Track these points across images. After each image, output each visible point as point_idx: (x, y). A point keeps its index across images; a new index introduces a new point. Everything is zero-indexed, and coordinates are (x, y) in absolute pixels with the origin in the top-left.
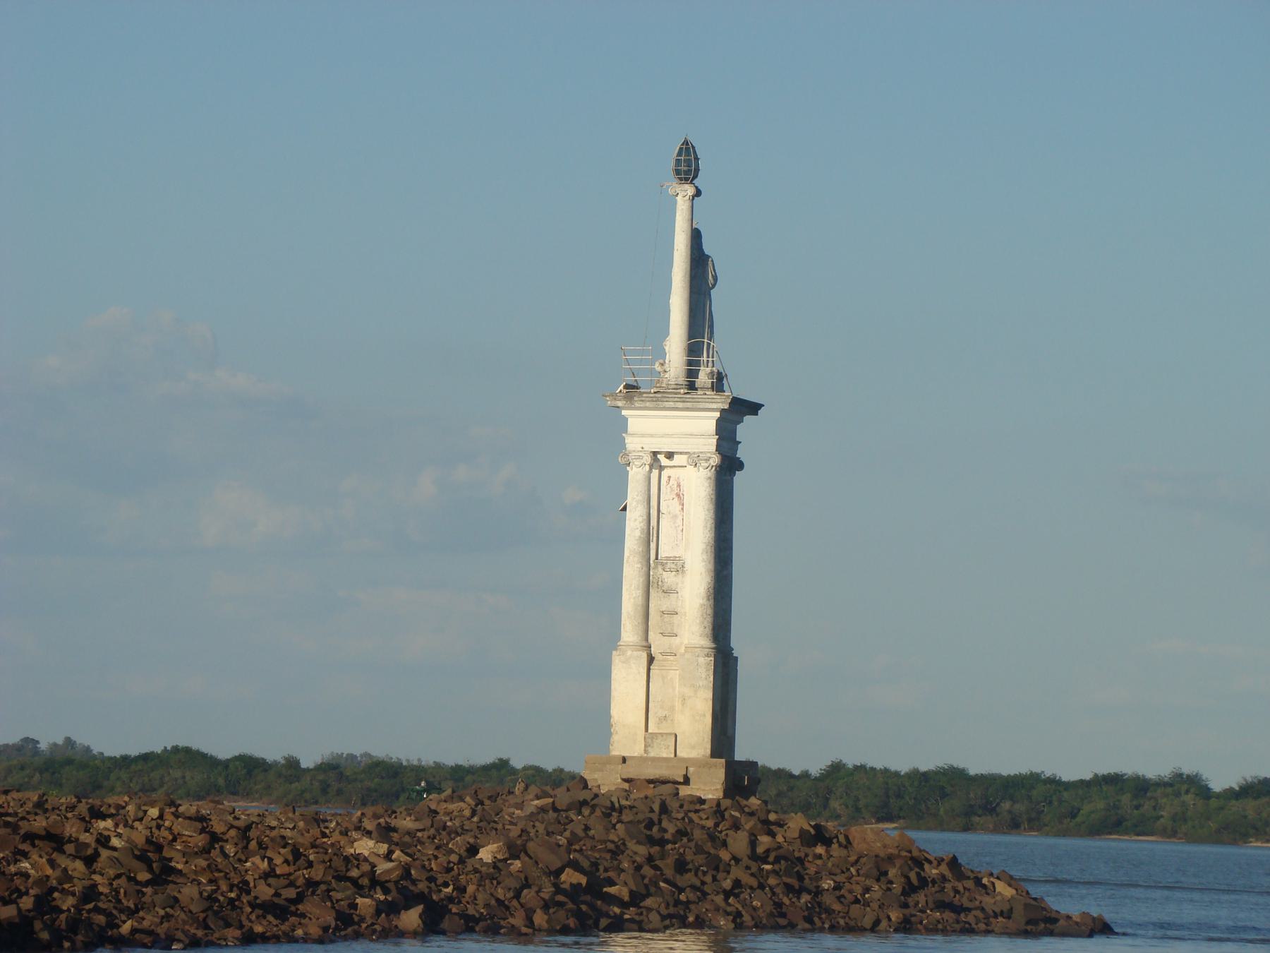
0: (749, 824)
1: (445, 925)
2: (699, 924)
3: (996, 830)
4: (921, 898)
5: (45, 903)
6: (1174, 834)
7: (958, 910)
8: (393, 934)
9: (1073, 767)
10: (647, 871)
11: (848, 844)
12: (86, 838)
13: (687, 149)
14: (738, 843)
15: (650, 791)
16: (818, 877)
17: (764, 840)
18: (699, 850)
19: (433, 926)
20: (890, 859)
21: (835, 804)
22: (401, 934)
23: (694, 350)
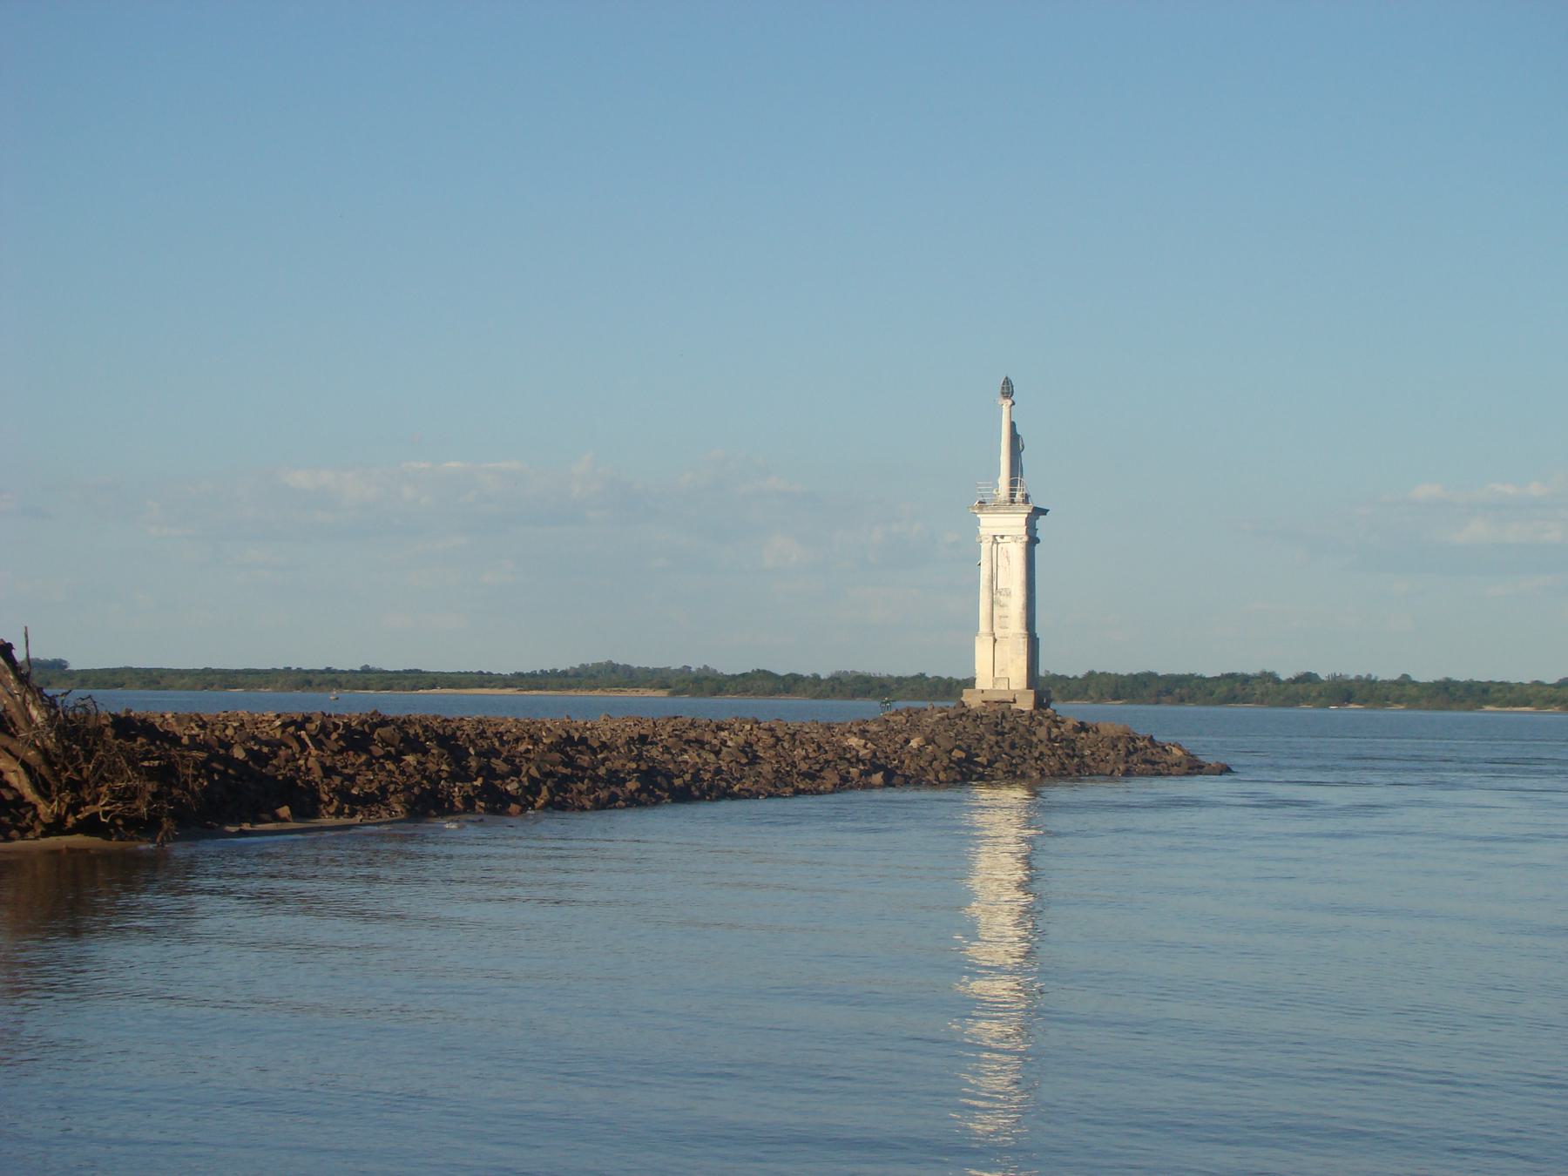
0: (1047, 723)
1: (895, 780)
2: (1023, 776)
3: (1172, 703)
4: (1134, 758)
5: (696, 777)
6: (1262, 702)
7: (1154, 763)
8: (869, 786)
9: (1210, 671)
10: (996, 749)
11: (1097, 731)
12: (715, 742)
13: (1007, 381)
14: (1042, 733)
15: (996, 707)
16: (1082, 749)
17: (1055, 731)
18: (1022, 737)
19: (888, 782)
20: (1119, 738)
21: (1091, 693)
22: (872, 787)
23: (1013, 483)
